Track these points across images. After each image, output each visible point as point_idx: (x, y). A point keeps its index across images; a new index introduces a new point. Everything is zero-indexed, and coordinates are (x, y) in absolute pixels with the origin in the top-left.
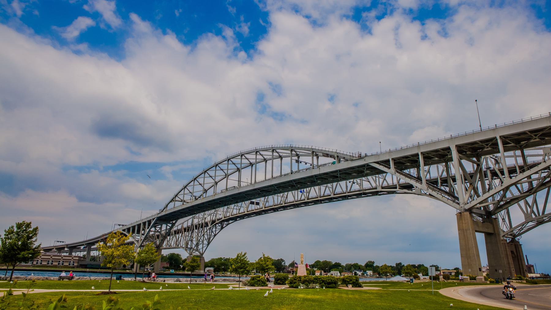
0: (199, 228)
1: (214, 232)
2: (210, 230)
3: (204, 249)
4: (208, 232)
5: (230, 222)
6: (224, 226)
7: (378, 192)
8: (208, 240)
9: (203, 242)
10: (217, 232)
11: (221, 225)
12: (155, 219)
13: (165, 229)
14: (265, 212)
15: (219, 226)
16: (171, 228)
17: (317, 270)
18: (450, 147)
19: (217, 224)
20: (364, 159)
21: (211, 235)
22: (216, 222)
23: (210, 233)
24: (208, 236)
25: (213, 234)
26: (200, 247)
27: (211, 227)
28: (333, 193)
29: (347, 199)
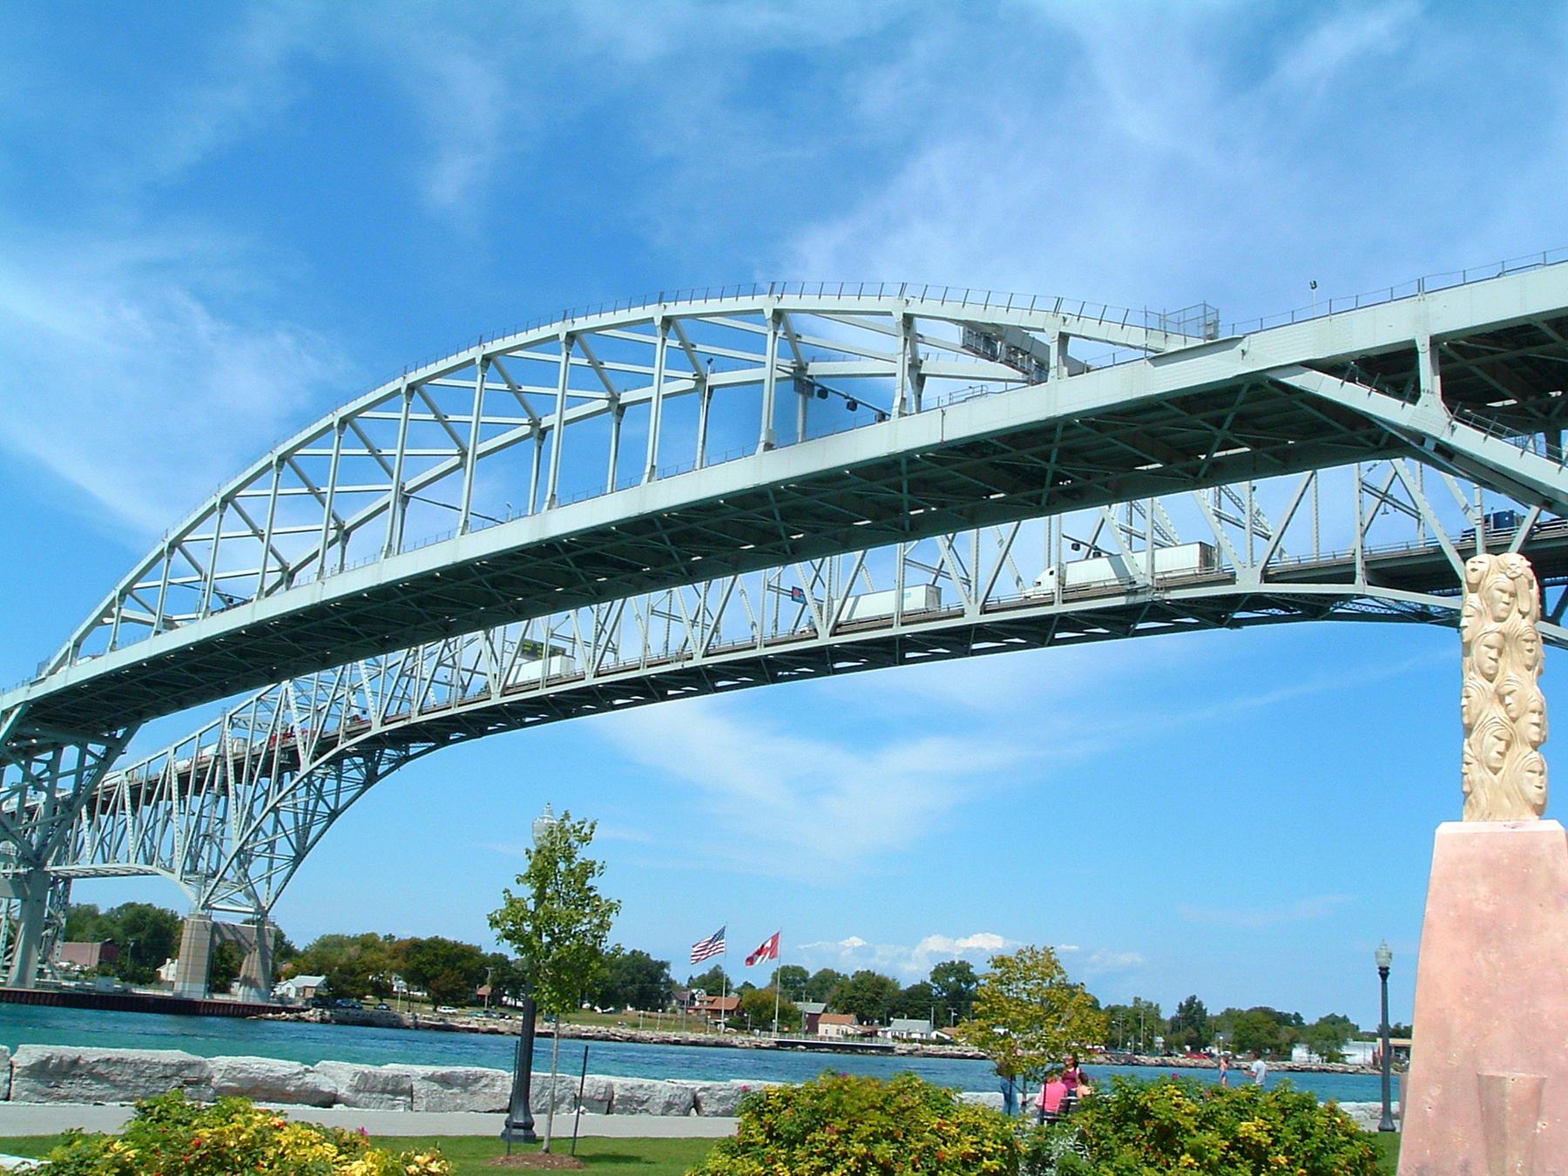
1: (331, 800)
2: (308, 785)
3: (277, 880)
4: (301, 792)
6: (381, 770)
7: (1234, 601)
8: (298, 838)
9: (271, 845)
10: (345, 797)
11: (365, 763)
12: (17, 711)
13: (75, 767)
14: (599, 698)
15: (357, 767)
16: (105, 763)
17: (825, 1011)
19: (343, 754)
20: (1240, 346)
21: (314, 810)
22: (340, 747)
23: (312, 803)
24: (301, 817)
25: (322, 807)
26: (258, 867)
27: (311, 774)
28: (980, 603)
29: (1049, 645)
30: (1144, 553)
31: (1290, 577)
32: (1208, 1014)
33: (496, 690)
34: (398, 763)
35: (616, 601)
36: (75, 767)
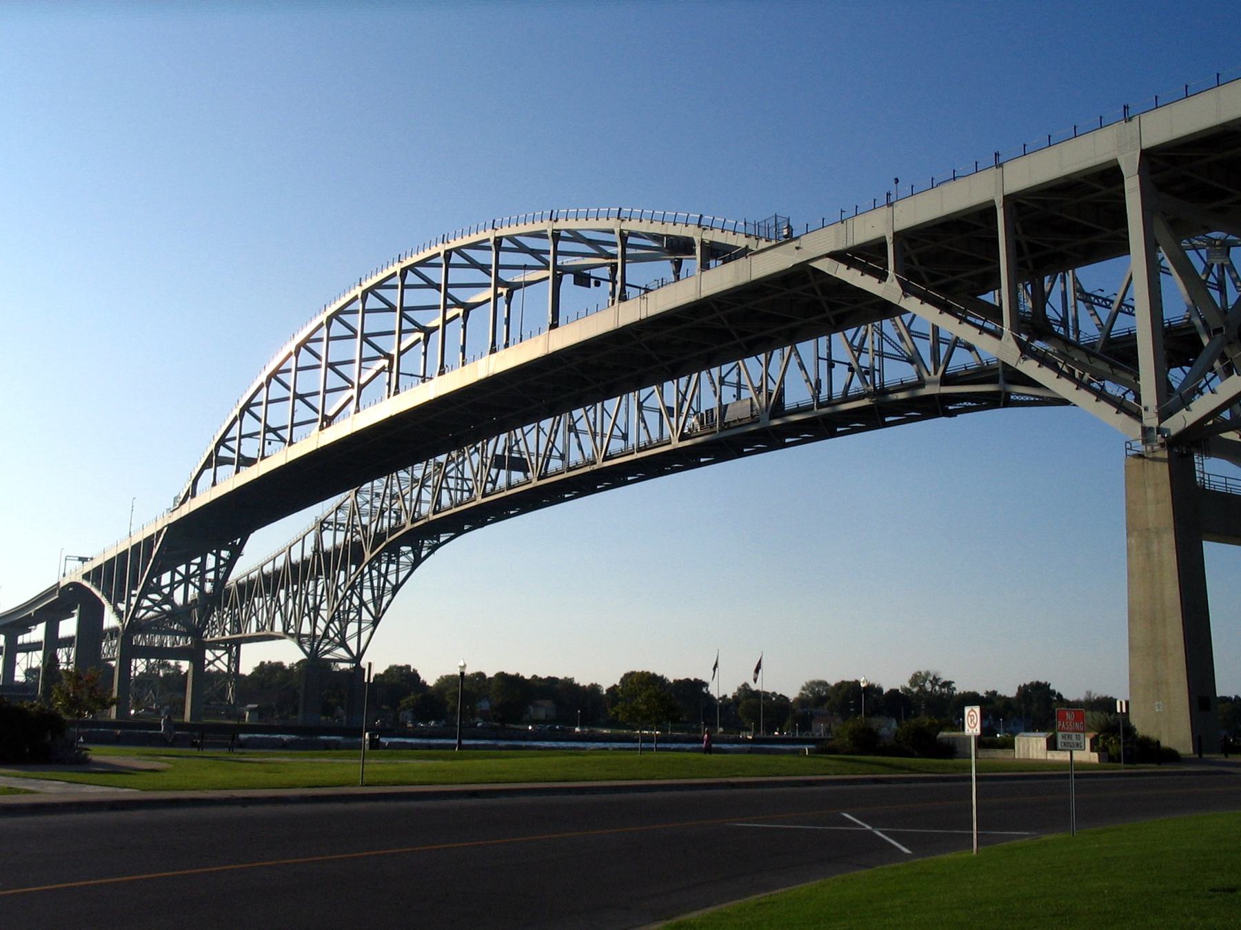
0: (303, 581)
5: (442, 540)
10: (402, 575)
15: (385, 556)
18: (1119, 167)
24: (376, 591)
27: (371, 561)
30: (947, 346)
31: (968, 379)
32: (863, 685)
33: (477, 493)
34: (433, 549)
35: (501, 436)
36: (1178, 368)
